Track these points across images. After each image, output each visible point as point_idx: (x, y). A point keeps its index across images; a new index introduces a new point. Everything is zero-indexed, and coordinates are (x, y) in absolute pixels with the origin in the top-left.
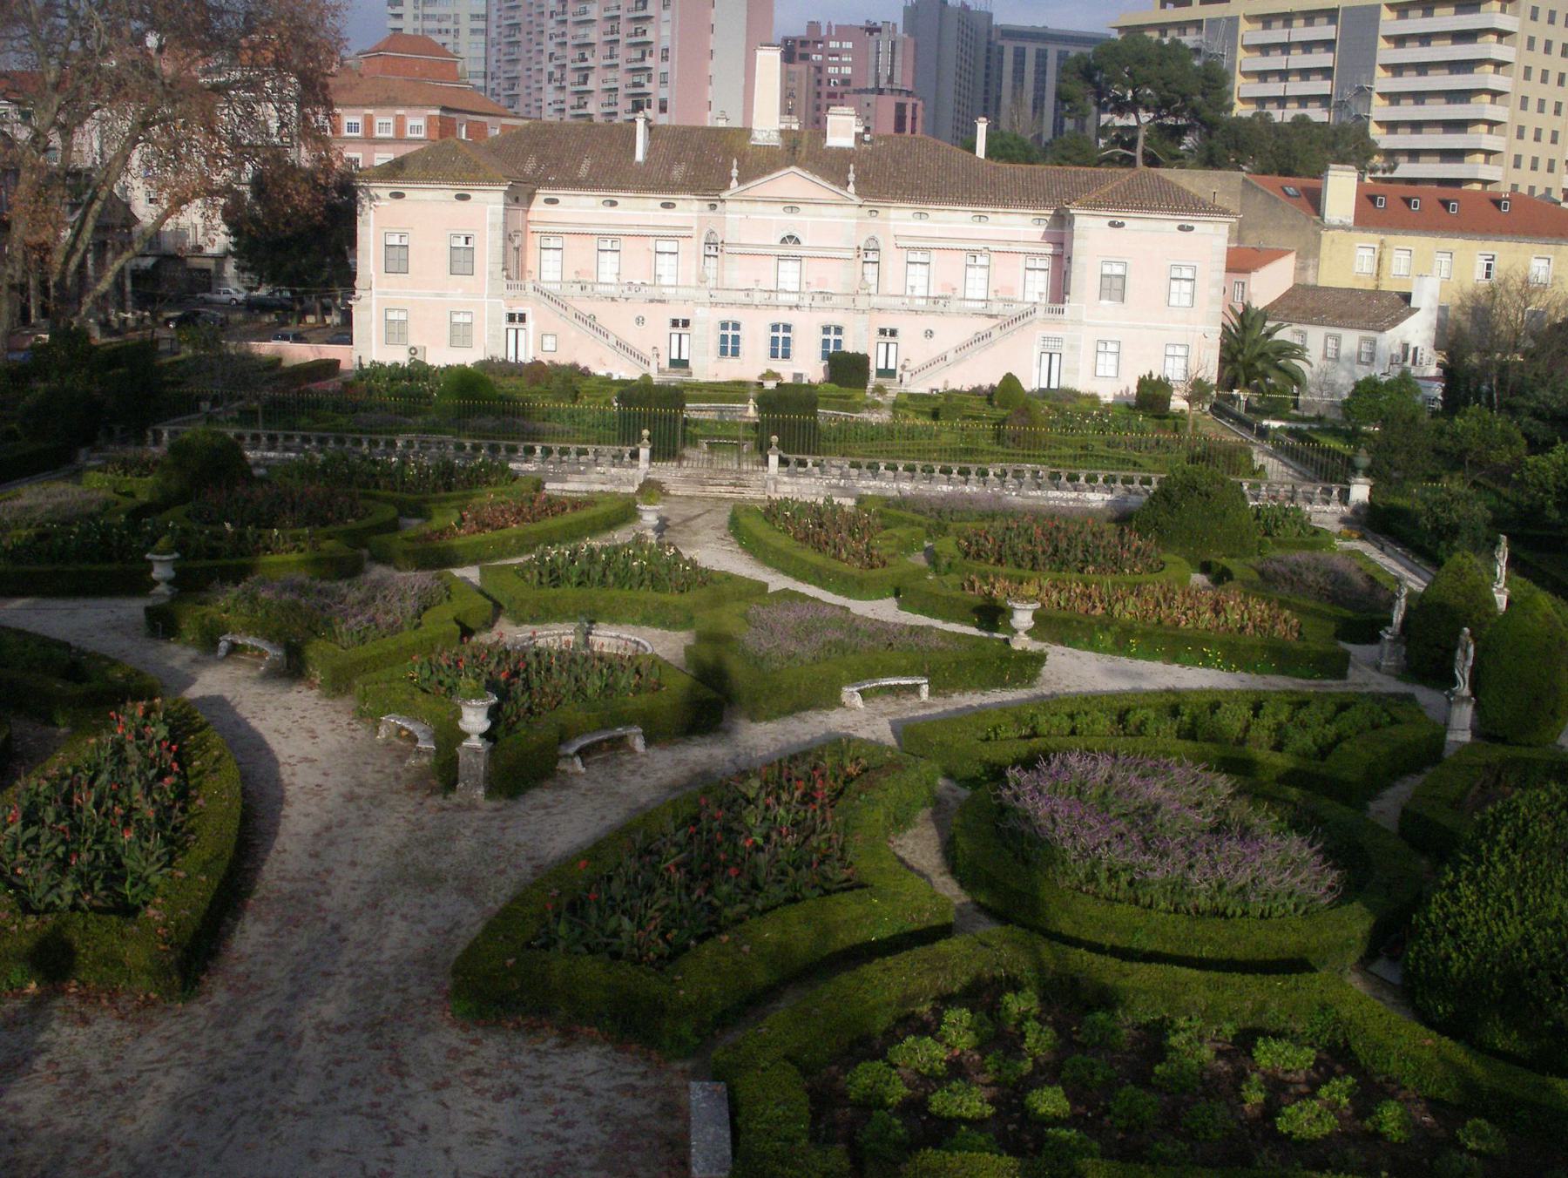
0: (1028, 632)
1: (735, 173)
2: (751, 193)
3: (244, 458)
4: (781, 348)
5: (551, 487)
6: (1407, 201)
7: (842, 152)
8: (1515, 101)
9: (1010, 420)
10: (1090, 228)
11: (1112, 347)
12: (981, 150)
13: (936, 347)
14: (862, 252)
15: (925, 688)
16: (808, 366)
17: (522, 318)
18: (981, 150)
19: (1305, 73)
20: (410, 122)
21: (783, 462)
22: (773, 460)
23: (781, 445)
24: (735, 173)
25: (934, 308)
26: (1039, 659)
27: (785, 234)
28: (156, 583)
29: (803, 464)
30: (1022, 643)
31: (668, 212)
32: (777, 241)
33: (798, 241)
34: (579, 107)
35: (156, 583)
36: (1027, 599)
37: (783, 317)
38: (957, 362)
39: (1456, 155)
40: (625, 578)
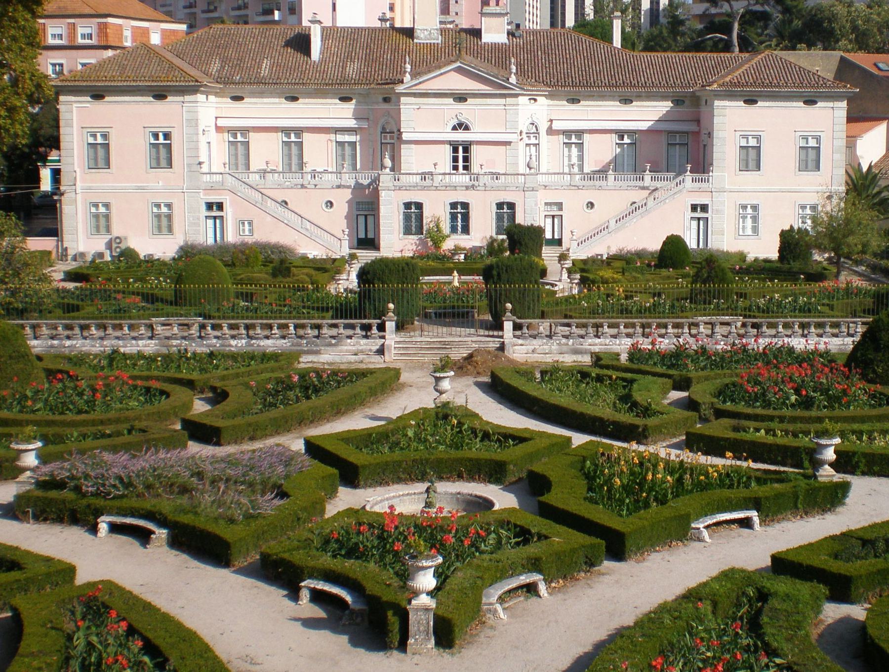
0: (831, 465)
1: (408, 67)
2: (423, 88)
3: (28, 347)
5: (306, 361)
7: (496, 48)
10: (210, 97)
12: (617, 41)
13: (596, 217)
14: (524, 135)
15: (756, 520)
17: (220, 206)
18: (617, 41)
20: (80, 31)
21: (517, 327)
23: (513, 312)
25: (424, 183)
26: (843, 488)
27: (455, 122)
28: (23, 470)
29: (120, 327)
30: (827, 474)
32: (449, 129)
33: (467, 128)
34: (209, 11)
35: (23, 470)
36: (29, 440)
38: (617, 230)
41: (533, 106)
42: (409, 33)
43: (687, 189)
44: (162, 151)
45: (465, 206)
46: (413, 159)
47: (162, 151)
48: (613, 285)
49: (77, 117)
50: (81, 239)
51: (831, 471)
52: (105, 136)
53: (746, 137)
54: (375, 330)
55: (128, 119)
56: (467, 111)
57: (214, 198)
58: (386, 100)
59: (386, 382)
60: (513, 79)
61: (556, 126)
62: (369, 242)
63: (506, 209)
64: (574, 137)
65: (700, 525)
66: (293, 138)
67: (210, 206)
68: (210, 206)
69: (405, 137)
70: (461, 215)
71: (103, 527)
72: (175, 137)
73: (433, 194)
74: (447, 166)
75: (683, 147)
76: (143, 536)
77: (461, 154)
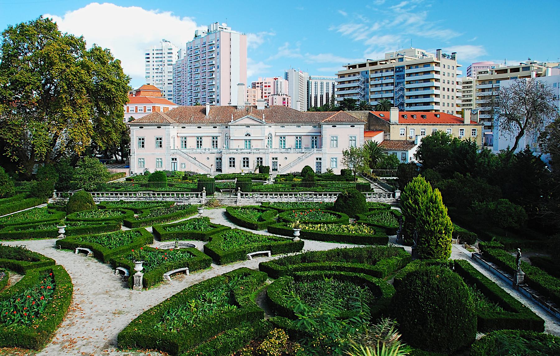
1: (232, 117)
4: (246, 162)
6: (412, 116)
8: (441, 89)
9: (308, 179)
11: (334, 160)
13: (287, 162)
15: (270, 254)
16: (252, 167)
17: (176, 159)
19: (387, 84)
21: (242, 195)
22: (239, 194)
24: (232, 117)
27: (246, 133)
28: (60, 234)
31: (215, 129)
35: (60, 234)
37: (246, 156)
39: (428, 104)
40: (269, 248)
41: (270, 129)
42: (236, 107)
43: (315, 153)
44: (160, 142)
45: (247, 159)
46: (234, 145)
47: (160, 142)
48: (289, 183)
49: (135, 134)
50: (136, 169)
51: (299, 239)
52: (158, 139)
53: (333, 137)
54: (199, 195)
55: (150, 134)
56: (249, 130)
57: (319, 157)
58: (227, 127)
59: (195, 210)
60: (264, 120)
61: (277, 134)
62: (219, 170)
63: (260, 160)
64: (283, 138)
65: (249, 255)
66: (283, 138)
67: (173, 159)
68: (173, 159)
69: (231, 138)
70: (246, 162)
71: (77, 251)
72: (163, 139)
73: (237, 155)
74: (196, 147)
75: (316, 141)
76: (86, 253)
77: (215, 143)
